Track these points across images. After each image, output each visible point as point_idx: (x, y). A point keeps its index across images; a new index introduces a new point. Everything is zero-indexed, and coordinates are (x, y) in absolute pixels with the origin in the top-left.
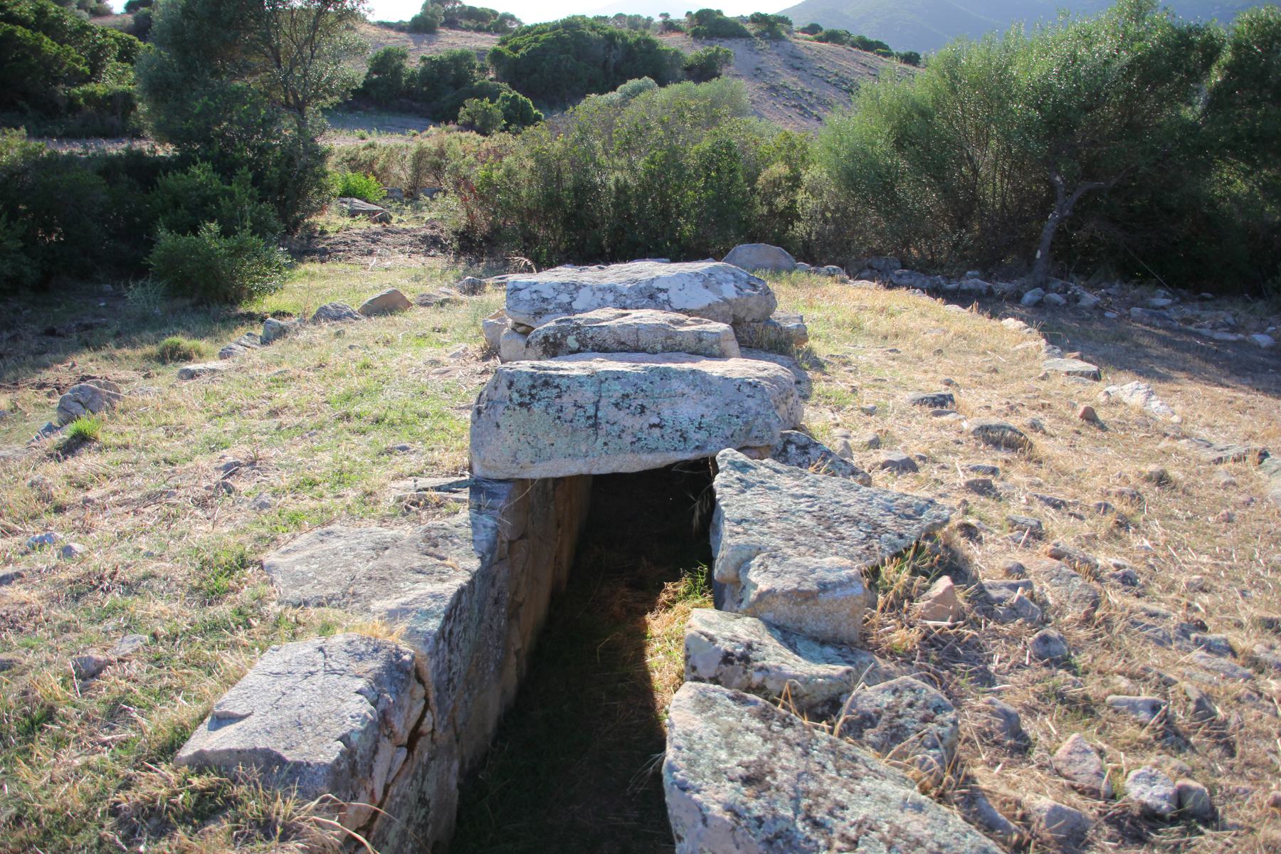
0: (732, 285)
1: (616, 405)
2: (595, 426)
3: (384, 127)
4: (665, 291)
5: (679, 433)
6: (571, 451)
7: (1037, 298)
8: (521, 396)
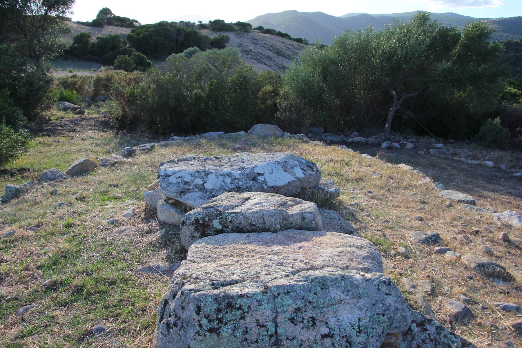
0: (299, 167)
1: (292, 320)
3: (81, 67)
4: (262, 175)
5: (345, 339)
8: (210, 321)
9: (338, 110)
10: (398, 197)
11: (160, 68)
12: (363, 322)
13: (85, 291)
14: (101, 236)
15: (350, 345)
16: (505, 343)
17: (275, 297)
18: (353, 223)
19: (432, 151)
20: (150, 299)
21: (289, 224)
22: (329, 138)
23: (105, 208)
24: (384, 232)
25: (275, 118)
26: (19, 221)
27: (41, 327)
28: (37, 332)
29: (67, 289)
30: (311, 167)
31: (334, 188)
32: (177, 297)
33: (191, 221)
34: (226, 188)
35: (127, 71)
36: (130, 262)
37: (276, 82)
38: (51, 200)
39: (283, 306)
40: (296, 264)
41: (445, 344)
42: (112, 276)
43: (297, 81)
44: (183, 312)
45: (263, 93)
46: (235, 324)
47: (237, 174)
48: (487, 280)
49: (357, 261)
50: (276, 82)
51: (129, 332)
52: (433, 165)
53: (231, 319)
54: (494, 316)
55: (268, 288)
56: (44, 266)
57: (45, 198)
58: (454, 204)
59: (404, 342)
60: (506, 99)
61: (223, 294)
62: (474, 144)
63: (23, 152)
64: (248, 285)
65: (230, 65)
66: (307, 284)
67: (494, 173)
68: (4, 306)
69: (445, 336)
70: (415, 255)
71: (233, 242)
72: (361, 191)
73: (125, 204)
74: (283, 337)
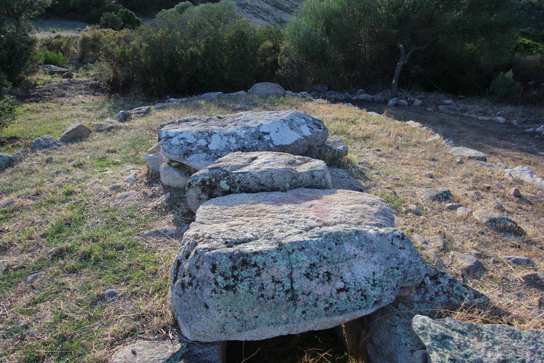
0: (306, 125)
1: (307, 275)
2: (294, 298)
4: (268, 134)
5: (360, 293)
6: (273, 321)
7: (395, 102)
8: (226, 279)
9: (343, 66)
10: (407, 155)
11: (151, 25)
12: (378, 276)
13: (93, 257)
14: (103, 202)
15: (366, 298)
16: (516, 294)
17: (289, 253)
18: (362, 182)
19: (441, 107)
20: (160, 262)
21: (298, 183)
22: (333, 96)
23: (105, 174)
24: (395, 189)
25: (276, 76)
26: (16, 191)
27: (52, 293)
28: (49, 299)
29: (74, 256)
30: (318, 125)
31: (342, 146)
32: (191, 257)
33: (197, 183)
34: (231, 148)
35: (115, 30)
36: (136, 227)
37: (276, 37)
38: (47, 168)
39: (298, 262)
40: (308, 221)
41: (458, 296)
42: (119, 241)
43: (299, 36)
44: (197, 272)
45: (263, 50)
46: (251, 280)
47: (242, 133)
48: (498, 234)
49: (370, 218)
50: (276, 37)
51: (142, 295)
52: (442, 123)
53: (247, 276)
54: (505, 269)
55: (282, 244)
56: (48, 235)
57: (41, 166)
58: (464, 161)
59: (418, 295)
60: (519, 51)
61: (237, 252)
62: (484, 100)
63: (11, 120)
64: (262, 242)
65: (226, 20)
66: (322, 240)
67: (505, 129)
68: (12, 275)
69: (458, 288)
70: (426, 212)
71: (242, 202)
72: (369, 149)
73: (125, 170)
74: (299, 292)
